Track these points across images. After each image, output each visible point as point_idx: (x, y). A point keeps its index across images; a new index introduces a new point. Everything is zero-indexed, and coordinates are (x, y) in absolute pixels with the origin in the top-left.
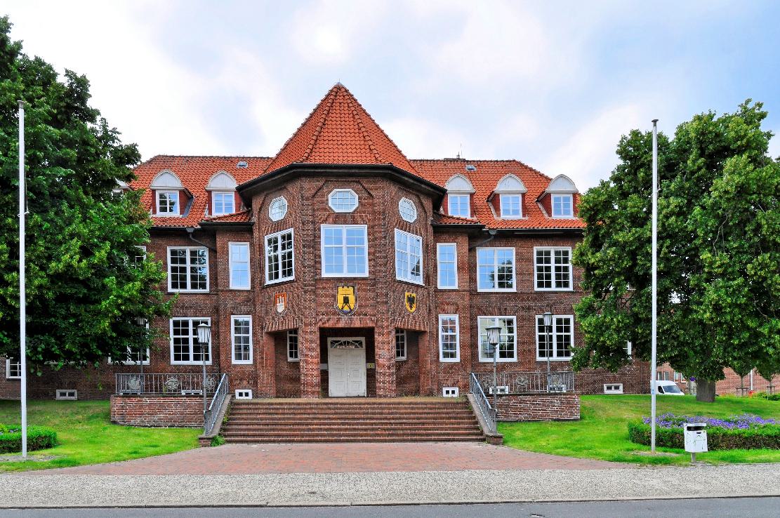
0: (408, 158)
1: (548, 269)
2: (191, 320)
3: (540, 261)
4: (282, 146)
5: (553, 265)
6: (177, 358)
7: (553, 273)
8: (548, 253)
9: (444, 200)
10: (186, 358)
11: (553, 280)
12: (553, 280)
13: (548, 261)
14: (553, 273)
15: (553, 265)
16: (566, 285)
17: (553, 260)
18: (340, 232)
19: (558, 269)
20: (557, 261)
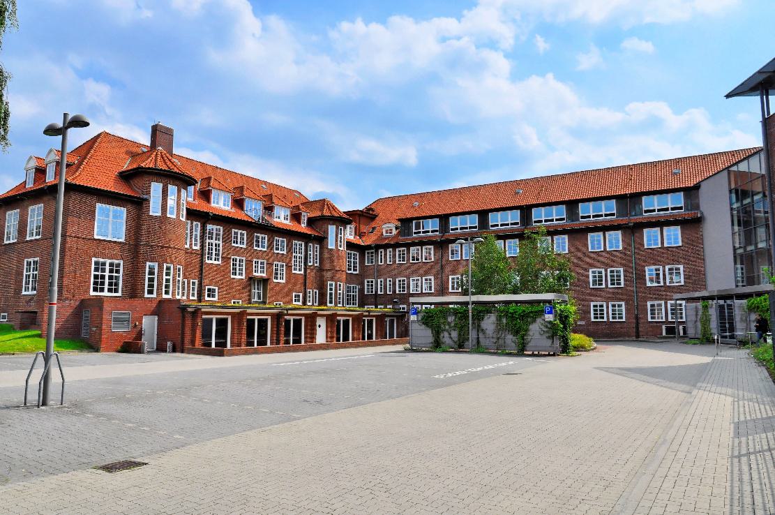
0: (69, 130)
1: (103, 277)
2: (108, 262)
3: (96, 269)
4: (751, 74)
5: (107, 274)
6: (95, 290)
7: (107, 281)
8: (104, 264)
9: (10, 194)
10: (102, 290)
11: (106, 287)
12: (106, 287)
13: (103, 270)
14: (107, 281)
15: (107, 274)
16: (116, 291)
17: (107, 270)
18: (109, 210)
19: (111, 278)
20: (111, 271)
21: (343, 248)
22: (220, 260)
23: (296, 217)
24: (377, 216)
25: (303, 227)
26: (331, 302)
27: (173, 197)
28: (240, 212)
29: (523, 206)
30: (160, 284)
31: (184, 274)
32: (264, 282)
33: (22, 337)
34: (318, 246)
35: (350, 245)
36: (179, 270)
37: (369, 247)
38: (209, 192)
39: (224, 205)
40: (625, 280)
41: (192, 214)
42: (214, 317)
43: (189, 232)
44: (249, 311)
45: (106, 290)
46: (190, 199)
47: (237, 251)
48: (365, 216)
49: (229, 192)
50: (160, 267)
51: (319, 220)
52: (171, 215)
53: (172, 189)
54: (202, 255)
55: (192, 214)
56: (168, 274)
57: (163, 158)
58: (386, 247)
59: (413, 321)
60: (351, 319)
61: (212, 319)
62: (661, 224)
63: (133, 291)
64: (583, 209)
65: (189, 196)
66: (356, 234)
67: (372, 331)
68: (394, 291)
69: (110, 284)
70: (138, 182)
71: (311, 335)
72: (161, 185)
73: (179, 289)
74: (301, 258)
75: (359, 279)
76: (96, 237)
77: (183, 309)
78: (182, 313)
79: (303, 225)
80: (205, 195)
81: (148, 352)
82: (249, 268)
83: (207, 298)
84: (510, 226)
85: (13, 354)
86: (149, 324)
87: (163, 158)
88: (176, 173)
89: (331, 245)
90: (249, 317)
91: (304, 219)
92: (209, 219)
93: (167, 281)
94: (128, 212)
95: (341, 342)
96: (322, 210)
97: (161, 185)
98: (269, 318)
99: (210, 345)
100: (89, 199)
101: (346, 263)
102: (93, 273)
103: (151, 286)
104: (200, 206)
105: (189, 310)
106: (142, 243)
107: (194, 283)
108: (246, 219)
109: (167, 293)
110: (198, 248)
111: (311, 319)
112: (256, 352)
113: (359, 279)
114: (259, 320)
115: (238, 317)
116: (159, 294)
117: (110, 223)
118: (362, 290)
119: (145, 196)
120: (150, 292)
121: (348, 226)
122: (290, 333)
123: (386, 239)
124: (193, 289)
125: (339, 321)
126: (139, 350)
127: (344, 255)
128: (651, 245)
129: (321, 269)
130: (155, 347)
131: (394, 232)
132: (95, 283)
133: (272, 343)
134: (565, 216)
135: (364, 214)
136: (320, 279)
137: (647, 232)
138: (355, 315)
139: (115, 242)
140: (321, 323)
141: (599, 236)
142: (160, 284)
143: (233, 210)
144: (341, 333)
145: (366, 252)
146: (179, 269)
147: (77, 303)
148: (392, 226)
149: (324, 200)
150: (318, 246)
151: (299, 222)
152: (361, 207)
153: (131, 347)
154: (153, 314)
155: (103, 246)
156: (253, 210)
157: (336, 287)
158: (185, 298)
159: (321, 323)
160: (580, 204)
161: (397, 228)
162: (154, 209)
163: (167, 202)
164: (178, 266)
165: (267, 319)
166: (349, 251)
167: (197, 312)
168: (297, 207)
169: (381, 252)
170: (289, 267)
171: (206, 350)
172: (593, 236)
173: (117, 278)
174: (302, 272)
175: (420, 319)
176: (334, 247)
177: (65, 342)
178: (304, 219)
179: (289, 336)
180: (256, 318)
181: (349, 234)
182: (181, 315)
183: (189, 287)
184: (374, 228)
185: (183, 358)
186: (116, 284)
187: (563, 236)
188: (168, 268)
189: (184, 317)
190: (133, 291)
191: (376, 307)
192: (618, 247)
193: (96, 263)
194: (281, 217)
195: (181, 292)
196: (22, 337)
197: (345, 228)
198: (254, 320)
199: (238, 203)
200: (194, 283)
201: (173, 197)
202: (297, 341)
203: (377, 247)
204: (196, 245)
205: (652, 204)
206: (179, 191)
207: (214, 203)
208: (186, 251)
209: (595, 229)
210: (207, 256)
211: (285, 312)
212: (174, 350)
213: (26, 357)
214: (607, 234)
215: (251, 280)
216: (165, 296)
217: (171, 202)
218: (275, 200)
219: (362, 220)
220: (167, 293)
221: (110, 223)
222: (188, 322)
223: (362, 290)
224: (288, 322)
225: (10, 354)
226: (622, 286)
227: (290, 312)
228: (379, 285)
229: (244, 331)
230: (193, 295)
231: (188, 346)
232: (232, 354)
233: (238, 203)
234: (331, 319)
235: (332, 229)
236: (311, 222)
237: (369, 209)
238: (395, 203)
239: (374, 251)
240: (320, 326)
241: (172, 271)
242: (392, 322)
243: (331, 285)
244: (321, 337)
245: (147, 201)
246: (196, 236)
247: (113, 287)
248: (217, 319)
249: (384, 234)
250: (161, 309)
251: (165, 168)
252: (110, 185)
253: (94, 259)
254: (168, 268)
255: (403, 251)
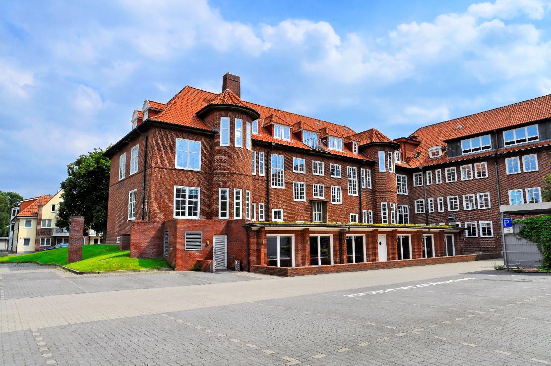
1: (184, 202)
3: (178, 196)
7: (187, 206)
12: (187, 211)
14: (187, 206)
19: (190, 203)
21: (392, 171)
22: (284, 184)
23: (348, 146)
24: (420, 142)
25: (355, 154)
26: (365, 222)
27: (239, 129)
28: (299, 143)
29: (493, 131)
30: (231, 207)
31: (253, 197)
32: (324, 203)
33: (116, 257)
34: (370, 170)
35: (399, 169)
36: (248, 195)
37: (417, 170)
38: (271, 126)
39: (285, 137)
40: (491, 204)
41: (256, 144)
42: (278, 236)
43: (255, 161)
44: (311, 229)
45: (187, 213)
46: (256, 133)
47: (298, 177)
48: (412, 142)
49: (288, 125)
50: (231, 193)
51: (369, 148)
52: (238, 144)
53: (238, 122)
54: (268, 181)
55: (256, 144)
56: (238, 198)
57: (230, 96)
58: (433, 168)
59: (506, 235)
60: (410, 235)
61: (276, 238)
62: (520, 153)
63: (209, 214)
64: (506, 137)
65: (254, 129)
66: (402, 160)
67: (431, 249)
68: (446, 210)
69: (190, 208)
70: (210, 118)
71: (374, 254)
72: (228, 119)
73: (248, 211)
74: (357, 181)
75: (409, 200)
76: (177, 167)
77: (248, 227)
78: (247, 231)
79: (354, 153)
80: (268, 129)
81: (217, 271)
82: (309, 194)
83: (274, 220)
84: (472, 152)
85: (99, 273)
86: (220, 243)
87: (230, 96)
88: (240, 107)
89: (382, 168)
90: (311, 235)
91: (355, 148)
92: (271, 149)
93: (238, 204)
94: (203, 145)
95: (454, 256)
96: (371, 137)
97: (228, 119)
98: (331, 236)
99: (275, 263)
100: (171, 134)
101: (398, 186)
102: (175, 199)
103: (224, 209)
104: (265, 138)
105: (254, 228)
106: (215, 172)
107: (261, 207)
108: (303, 147)
109: (238, 215)
110: (263, 175)
111: (372, 237)
112: (320, 271)
113: (409, 200)
114: (321, 238)
115: (302, 235)
116: (231, 216)
117: (188, 154)
118: (412, 210)
119: (217, 130)
120: (224, 215)
121: (396, 152)
122: (351, 252)
123: (433, 160)
124: (261, 212)
125: (399, 239)
126: (209, 270)
127: (394, 178)
128: (529, 169)
129: (373, 192)
130: (226, 265)
131: (441, 154)
132: (177, 208)
133: (335, 262)
134: (490, 144)
135: (409, 141)
136: (374, 197)
137: (525, 159)
138: (415, 232)
139: (192, 171)
140: (382, 239)
141: (517, 160)
142: (231, 207)
143: (293, 142)
144: (401, 252)
145: (414, 174)
146: (248, 194)
147: (160, 225)
148: (437, 148)
149: (372, 130)
150: (370, 170)
151: (351, 150)
152: (407, 135)
153: (202, 266)
154: (222, 233)
155: (184, 175)
156: (310, 141)
157: (391, 208)
158: (254, 220)
159: (382, 239)
160: (504, 133)
161: (443, 150)
162: (224, 141)
163: (236, 135)
164: (247, 191)
165: (431, 236)
166: (397, 175)
167: (260, 231)
168: (349, 138)
169: (429, 174)
170: (345, 190)
171: (271, 269)
172: (510, 161)
173: (196, 203)
174: (357, 195)
175: (517, 231)
176: (384, 171)
177: (146, 262)
178: (355, 148)
179: (352, 254)
180: (319, 236)
181: (396, 159)
182: (246, 232)
183: (257, 209)
184: (419, 153)
185: (247, 279)
186: (196, 209)
187: (515, 158)
188: (238, 193)
189: (248, 237)
190: (209, 214)
191: (428, 224)
192: (535, 168)
193: (178, 190)
194: (336, 146)
195: (250, 213)
196: (116, 257)
197: (393, 153)
198: (316, 238)
199: (297, 135)
200: (261, 207)
201: (239, 129)
202: (359, 259)
203: (425, 169)
204: (262, 172)
205: (511, 137)
206: (244, 124)
207: (276, 135)
208: (254, 178)
209: (511, 154)
210: (272, 182)
211: (347, 229)
212: (242, 269)
213: (92, 277)
214: (524, 157)
215: (312, 201)
216: (236, 218)
217: (238, 134)
218: (328, 131)
219: (407, 147)
220: (238, 215)
221: (188, 154)
222: (253, 240)
223: (412, 210)
224: (349, 241)
225: (95, 273)
226: (490, 207)
227: (352, 229)
228: (435, 204)
229: (345, 248)
230: (261, 217)
231: (253, 265)
232: (296, 273)
233: (297, 135)
234: (391, 236)
235: (381, 154)
236: (361, 150)
237: (412, 137)
238: (436, 129)
239: (422, 173)
240: (380, 244)
241: (241, 196)
242: (449, 238)
243: (384, 205)
244: (382, 255)
245: (218, 133)
246: (262, 164)
247: (193, 211)
248: (281, 239)
249: (431, 157)
250: (229, 229)
251: (230, 102)
252: (188, 121)
253: (175, 187)
254: (224, 192)
255: (420, 175)
